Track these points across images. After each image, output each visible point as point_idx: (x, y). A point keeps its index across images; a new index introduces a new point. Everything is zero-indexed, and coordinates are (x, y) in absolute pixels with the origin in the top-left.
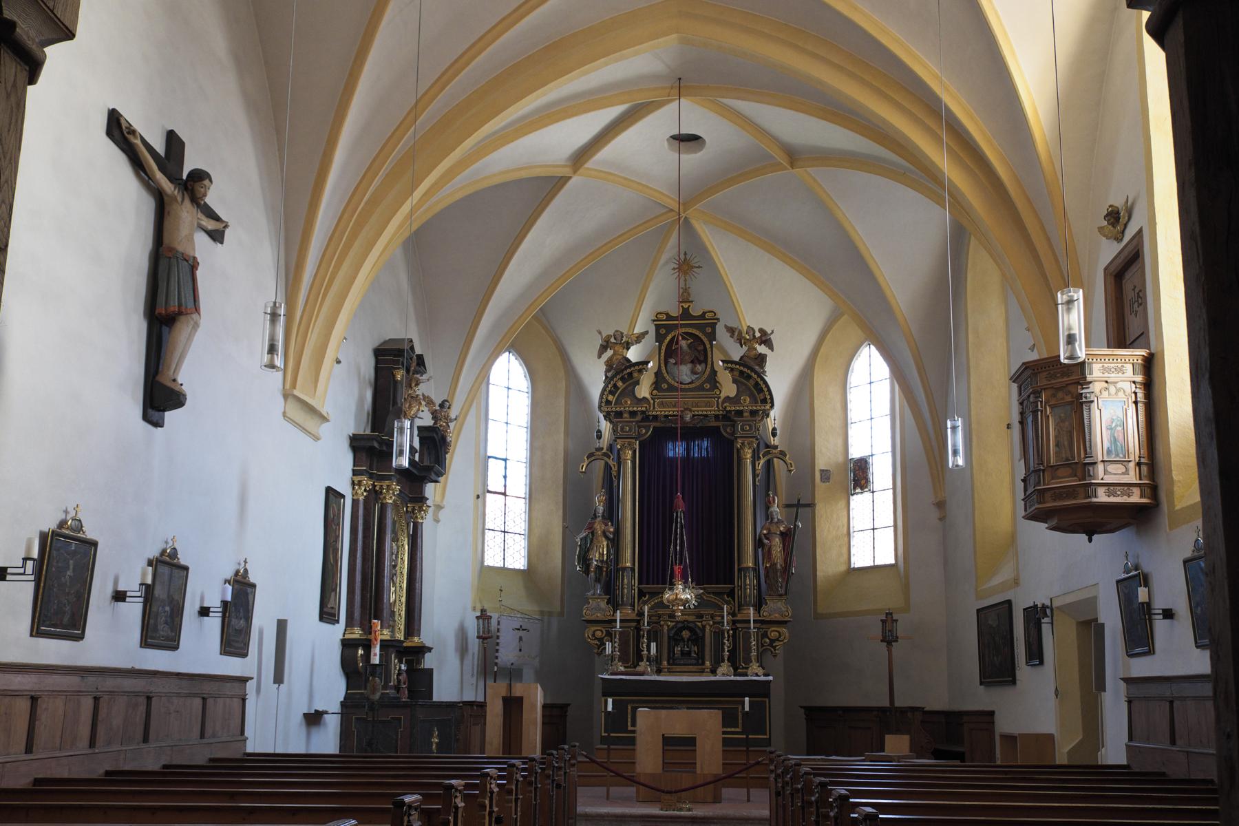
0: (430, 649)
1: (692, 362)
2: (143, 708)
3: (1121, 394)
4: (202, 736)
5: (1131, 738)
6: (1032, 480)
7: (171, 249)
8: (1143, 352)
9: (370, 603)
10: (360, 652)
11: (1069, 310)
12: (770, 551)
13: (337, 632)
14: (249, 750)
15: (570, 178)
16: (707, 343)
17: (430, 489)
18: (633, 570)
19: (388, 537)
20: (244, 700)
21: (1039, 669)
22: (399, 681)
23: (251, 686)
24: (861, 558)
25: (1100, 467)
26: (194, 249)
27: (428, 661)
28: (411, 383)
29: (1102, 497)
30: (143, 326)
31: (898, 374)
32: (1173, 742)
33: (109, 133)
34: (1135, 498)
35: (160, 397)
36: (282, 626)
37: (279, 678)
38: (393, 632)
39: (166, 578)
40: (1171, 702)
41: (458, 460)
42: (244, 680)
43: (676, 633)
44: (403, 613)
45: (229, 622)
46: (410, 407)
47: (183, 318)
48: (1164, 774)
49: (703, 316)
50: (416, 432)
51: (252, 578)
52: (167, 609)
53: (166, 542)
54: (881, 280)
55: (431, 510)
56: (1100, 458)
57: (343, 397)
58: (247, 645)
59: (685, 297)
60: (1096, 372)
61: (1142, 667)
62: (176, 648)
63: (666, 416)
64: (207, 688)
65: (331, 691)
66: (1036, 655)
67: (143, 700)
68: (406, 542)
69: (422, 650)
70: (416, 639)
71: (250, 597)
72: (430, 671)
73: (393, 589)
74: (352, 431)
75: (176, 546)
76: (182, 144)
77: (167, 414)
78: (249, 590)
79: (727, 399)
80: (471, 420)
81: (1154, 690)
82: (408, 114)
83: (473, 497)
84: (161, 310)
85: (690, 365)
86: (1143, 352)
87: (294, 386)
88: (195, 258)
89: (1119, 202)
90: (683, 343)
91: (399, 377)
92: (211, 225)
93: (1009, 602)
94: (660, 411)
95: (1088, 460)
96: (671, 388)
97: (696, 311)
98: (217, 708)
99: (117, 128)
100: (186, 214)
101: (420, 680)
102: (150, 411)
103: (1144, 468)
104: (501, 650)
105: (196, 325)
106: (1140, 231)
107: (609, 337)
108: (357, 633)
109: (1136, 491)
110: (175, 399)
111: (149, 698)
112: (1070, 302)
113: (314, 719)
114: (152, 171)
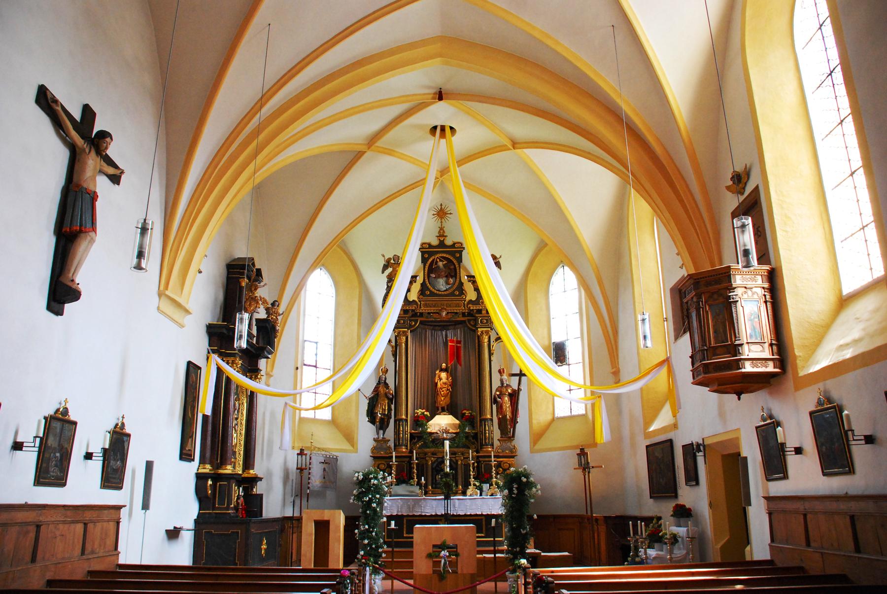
0: (261, 479)
1: (446, 276)
2: (32, 535)
3: (755, 296)
4: (83, 553)
5: (772, 540)
6: (698, 357)
7: (79, 186)
8: (767, 267)
9: (217, 445)
10: (210, 482)
11: (743, 232)
12: (501, 406)
13: (193, 467)
14: (122, 561)
15: (364, 153)
16: (456, 264)
17: (262, 363)
18: (407, 420)
19: (233, 398)
20: (118, 523)
21: (697, 487)
22: (238, 503)
23: (124, 512)
24: (562, 410)
25: (746, 347)
26: (95, 186)
27: (259, 489)
28: (253, 287)
29: (748, 368)
30: (53, 240)
31: (583, 283)
32: (808, 544)
33: (38, 101)
34: (770, 368)
35: (61, 293)
36: (149, 466)
37: (146, 506)
38: (234, 467)
39: (58, 430)
40: (805, 516)
41: (283, 343)
42: (118, 508)
43: (437, 466)
44: (242, 453)
45: (109, 463)
46: (250, 305)
47: (82, 235)
48: (801, 569)
49: (453, 246)
50: (254, 323)
51: (128, 430)
52: (58, 455)
53: (60, 403)
54: (572, 223)
55: (264, 378)
56: (745, 341)
57: (201, 295)
58: (121, 480)
59: (442, 235)
60: (738, 280)
61: (778, 488)
62: (64, 485)
63: (429, 313)
64: (88, 515)
65: (186, 511)
66: (692, 478)
67: (33, 529)
68: (245, 401)
69: (255, 480)
70: (251, 471)
71: (126, 444)
72: (260, 497)
73: (235, 435)
74: (209, 320)
75: (67, 406)
76: (94, 114)
77: (66, 306)
78: (125, 438)
79: (471, 302)
80: (293, 314)
81: (790, 506)
82: (256, 104)
83: (294, 368)
84: (66, 229)
85: (445, 279)
86: (767, 267)
87: (167, 287)
88: (95, 193)
89: (739, 168)
90: (440, 264)
91: (244, 284)
92: (111, 171)
93: (670, 441)
94: (423, 309)
95: (737, 342)
96: (432, 294)
97: (449, 242)
98: (96, 531)
99: (45, 99)
100: (92, 162)
101: (253, 503)
102: (53, 304)
103: (775, 348)
104: (312, 478)
105: (92, 241)
106: (757, 187)
107: (389, 259)
108: (207, 469)
109: (771, 364)
110: (75, 295)
111: (38, 527)
112: (743, 226)
113: (173, 534)
114: (67, 127)
